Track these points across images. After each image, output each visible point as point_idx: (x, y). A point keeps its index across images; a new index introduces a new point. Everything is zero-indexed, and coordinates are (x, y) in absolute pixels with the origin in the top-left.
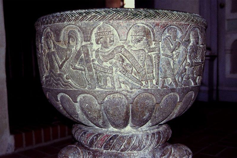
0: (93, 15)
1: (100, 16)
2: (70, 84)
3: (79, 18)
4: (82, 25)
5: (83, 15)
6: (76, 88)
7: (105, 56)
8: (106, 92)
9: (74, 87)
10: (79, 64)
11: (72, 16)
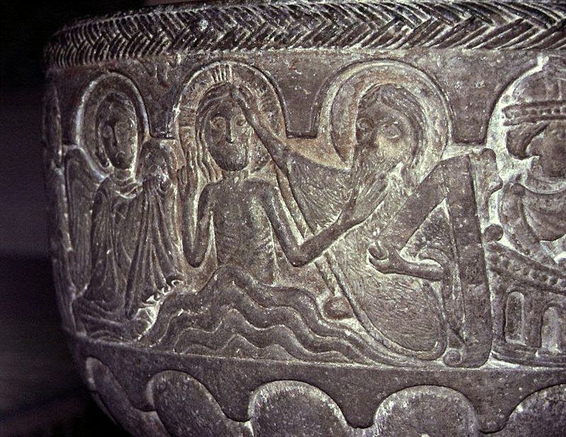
0: (510, 21)
1: (542, 31)
2: (350, 339)
3: (436, 34)
4: (444, 64)
5: (458, 19)
6: (387, 362)
7: (551, 213)
8: (531, 376)
9: (374, 357)
10: (419, 247)
11: (398, 18)
